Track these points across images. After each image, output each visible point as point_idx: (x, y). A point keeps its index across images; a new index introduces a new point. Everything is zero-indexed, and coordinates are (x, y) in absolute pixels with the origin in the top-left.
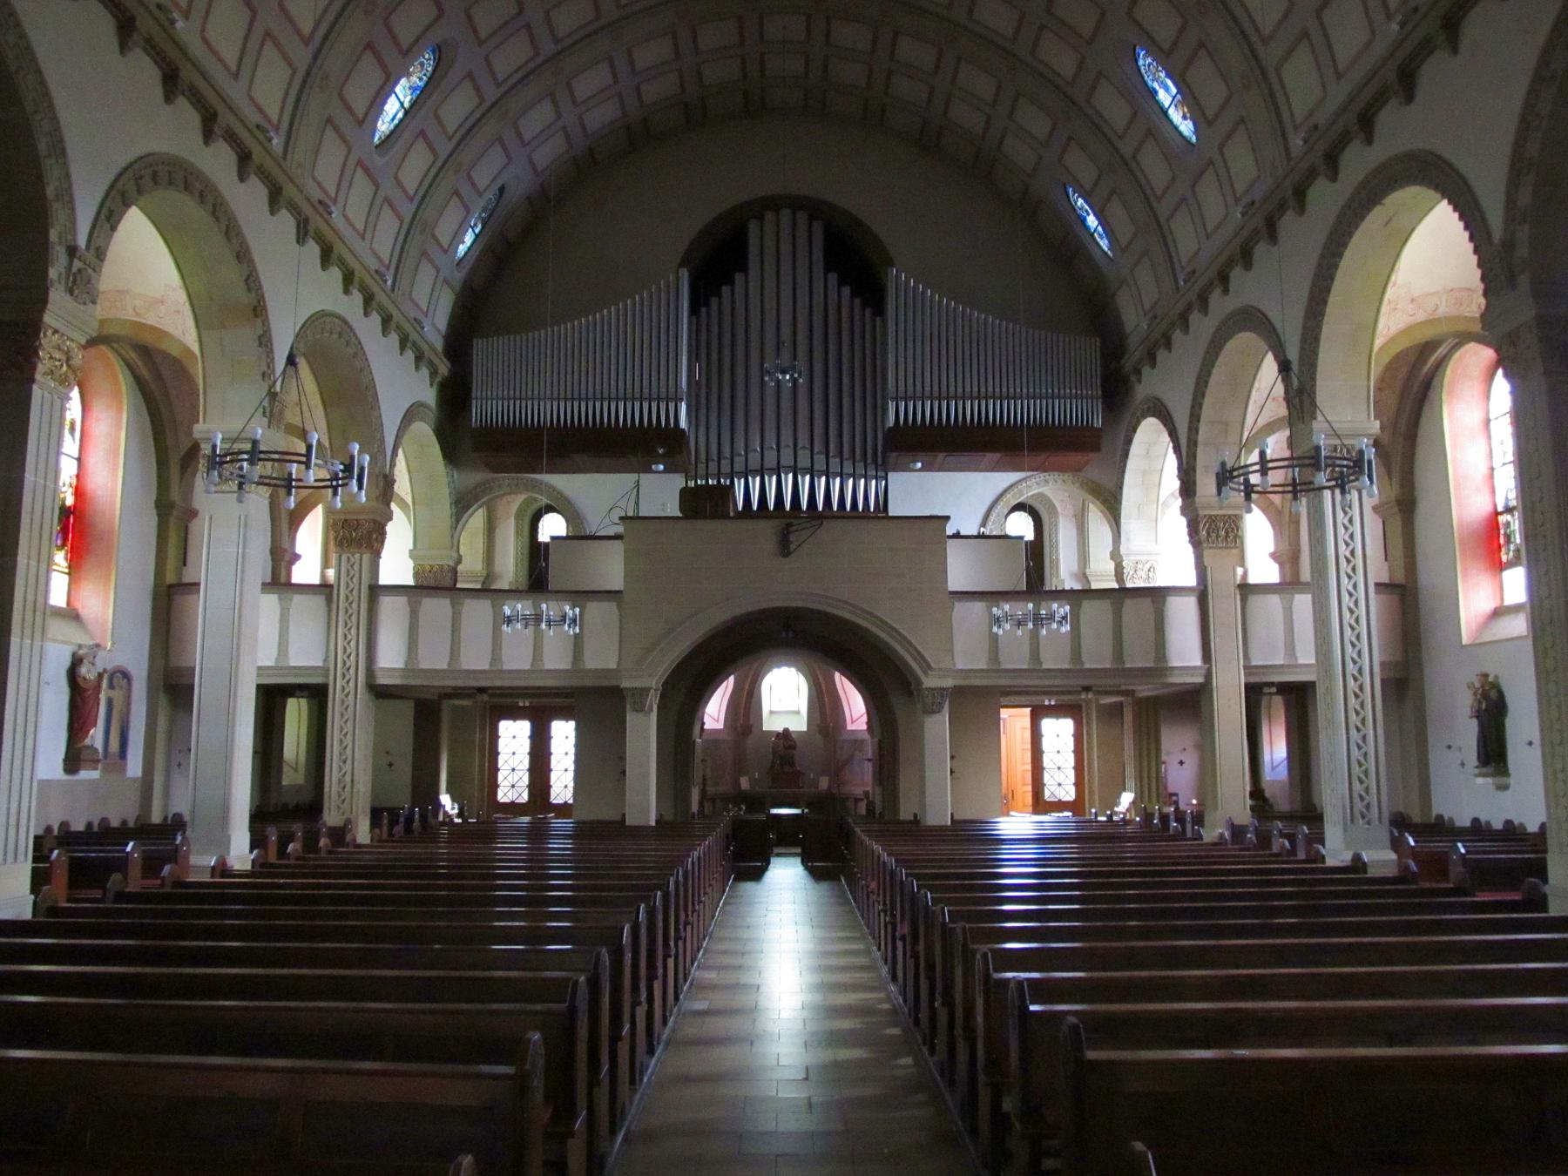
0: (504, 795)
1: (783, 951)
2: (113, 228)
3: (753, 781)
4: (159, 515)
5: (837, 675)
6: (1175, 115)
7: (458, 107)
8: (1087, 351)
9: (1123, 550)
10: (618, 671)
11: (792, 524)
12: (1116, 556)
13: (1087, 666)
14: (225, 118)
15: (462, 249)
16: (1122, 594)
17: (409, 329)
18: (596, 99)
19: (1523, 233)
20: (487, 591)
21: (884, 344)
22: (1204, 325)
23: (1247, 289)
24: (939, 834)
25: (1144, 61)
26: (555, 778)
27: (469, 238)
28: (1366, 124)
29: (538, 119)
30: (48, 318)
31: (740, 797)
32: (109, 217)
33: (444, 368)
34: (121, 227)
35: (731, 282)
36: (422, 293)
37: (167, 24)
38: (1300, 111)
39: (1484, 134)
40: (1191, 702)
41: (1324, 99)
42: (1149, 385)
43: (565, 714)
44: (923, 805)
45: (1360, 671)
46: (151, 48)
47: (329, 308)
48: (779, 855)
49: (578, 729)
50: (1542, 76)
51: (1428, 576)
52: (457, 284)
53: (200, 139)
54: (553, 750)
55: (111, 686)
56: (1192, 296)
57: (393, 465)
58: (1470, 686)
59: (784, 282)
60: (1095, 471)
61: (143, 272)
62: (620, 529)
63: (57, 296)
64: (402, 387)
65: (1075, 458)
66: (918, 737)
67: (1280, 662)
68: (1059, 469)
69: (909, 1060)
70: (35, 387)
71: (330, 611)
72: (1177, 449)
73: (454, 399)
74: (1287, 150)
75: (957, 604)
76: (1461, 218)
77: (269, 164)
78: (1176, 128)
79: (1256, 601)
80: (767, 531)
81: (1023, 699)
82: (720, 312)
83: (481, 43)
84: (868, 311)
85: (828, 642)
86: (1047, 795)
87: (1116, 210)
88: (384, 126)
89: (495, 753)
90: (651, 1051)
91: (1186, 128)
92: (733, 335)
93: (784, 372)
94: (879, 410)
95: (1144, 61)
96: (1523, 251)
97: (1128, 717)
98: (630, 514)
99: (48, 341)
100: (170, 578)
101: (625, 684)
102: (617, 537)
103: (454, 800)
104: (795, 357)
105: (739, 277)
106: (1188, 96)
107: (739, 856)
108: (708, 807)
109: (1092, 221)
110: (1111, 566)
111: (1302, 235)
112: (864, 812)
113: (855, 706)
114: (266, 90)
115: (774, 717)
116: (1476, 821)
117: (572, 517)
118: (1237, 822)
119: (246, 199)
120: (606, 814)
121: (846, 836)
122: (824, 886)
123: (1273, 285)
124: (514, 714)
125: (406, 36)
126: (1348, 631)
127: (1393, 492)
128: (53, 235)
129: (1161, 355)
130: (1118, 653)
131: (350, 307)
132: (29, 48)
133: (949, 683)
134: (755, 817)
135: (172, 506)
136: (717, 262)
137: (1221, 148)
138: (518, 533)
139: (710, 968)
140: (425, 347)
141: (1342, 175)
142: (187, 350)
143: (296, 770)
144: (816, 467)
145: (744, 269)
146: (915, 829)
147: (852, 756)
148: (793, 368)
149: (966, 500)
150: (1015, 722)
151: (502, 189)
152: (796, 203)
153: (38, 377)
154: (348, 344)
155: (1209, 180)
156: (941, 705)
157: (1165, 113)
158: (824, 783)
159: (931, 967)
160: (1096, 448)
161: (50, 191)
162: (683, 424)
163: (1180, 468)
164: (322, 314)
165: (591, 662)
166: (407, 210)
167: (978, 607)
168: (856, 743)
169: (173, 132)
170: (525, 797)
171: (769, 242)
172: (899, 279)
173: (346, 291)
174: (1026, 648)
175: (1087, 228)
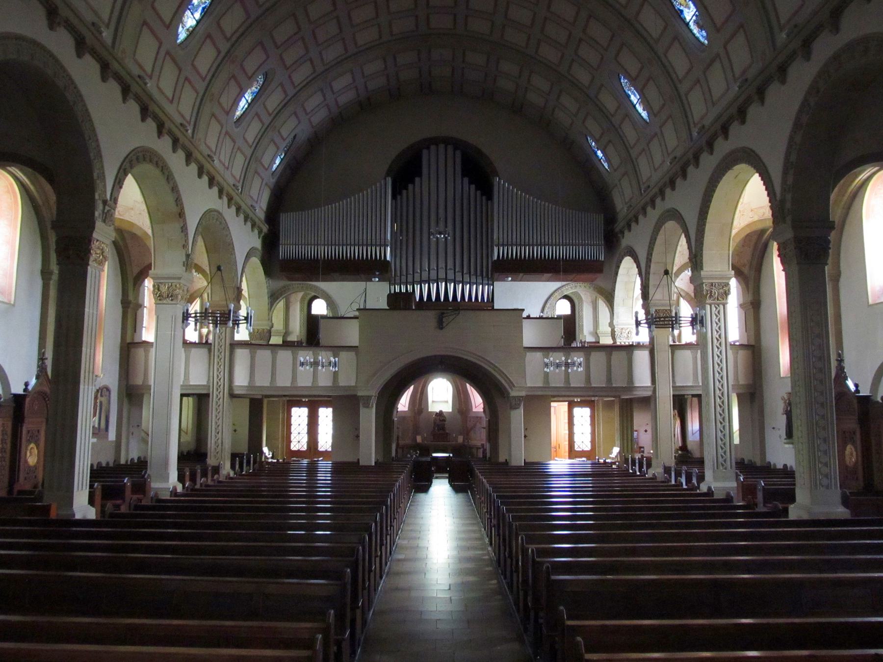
0: (294, 447)
1: (439, 530)
2: (121, 187)
3: (423, 439)
4: (123, 307)
5: (468, 385)
6: (640, 108)
7: (274, 101)
8: (598, 220)
9: (615, 322)
10: (355, 387)
11: (445, 310)
12: (611, 324)
13: (593, 385)
14: (168, 124)
15: (275, 166)
16: (614, 348)
17: (248, 211)
18: (344, 89)
19: (789, 197)
20: (287, 344)
21: (492, 216)
22: (653, 214)
23: (673, 200)
24: (518, 471)
25: (624, 81)
26: (294, 437)
27: (278, 162)
28: (725, 130)
29: (315, 101)
30: (95, 235)
31: (416, 446)
32: (119, 183)
33: (265, 228)
34: (124, 186)
35: (413, 183)
36: (254, 192)
37: (143, 86)
38: (697, 117)
39: (774, 144)
40: (648, 402)
41: (706, 114)
42: (627, 240)
43: (326, 404)
44: (510, 455)
45: (722, 394)
46: (138, 99)
47: (214, 207)
48: (437, 478)
49: (333, 412)
50: (797, 125)
51: (766, 341)
52: (272, 186)
53: (156, 135)
54: (320, 422)
55: (101, 396)
56: (648, 199)
57: (241, 281)
58: (783, 398)
59: (440, 180)
60: (601, 281)
61: (131, 202)
62: (357, 313)
63: (99, 224)
64: (245, 240)
65: (590, 276)
66: (508, 419)
67: (690, 384)
68: (583, 281)
69: (495, 582)
70: (89, 267)
71: (210, 357)
72: (640, 274)
73: (271, 242)
74: (691, 135)
75: (528, 354)
76: (764, 184)
77: (187, 143)
78: (640, 114)
79: (679, 354)
80: (431, 316)
81: (566, 399)
82: (407, 198)
83: (277, 47)
84: (484, 198)
85: (464, 371)
86: (577, 448)
87: (610, 149)
88: (238, 113)
89: (289, 425)
90: (381, 577)
91: (644, 114)
92: (414, 208)
93: (440, 234)
94: (490, 253)
95: (624, 81)
96: (788, 205)
97: (617, 408)
98: (362, 307)
99: (95, 245)
100: (129, 340)
101: (360, 394)
102: (355, 318)
103: (269, 450)
104: (446, 227)
105: (417, 179)
106: (644, 100)
107: (417, 479)
108: (400, 451)
109: (599, 153)
110: (610, 329)
111: (698, 176)
112: (481, 456)
113: (477, 401)
114: (184, 107)
115: (435, 404)
116: (785, 466)
117: (331, 304)
118: (667, 465)
119: (176, 161)
120: (350, 458)
121: (471, 472)
122: (460, 495)
123: (683, 198)
124: (299, 404)
125: (250, 69)
126: (717, 375)
127: (750, 298)
128: (97, 197)
129: (633, 225)
130: (609, 380)
131: (220, 205)
132: (87, 110)
133: (523, 394)
134: (424, 459)
135: (129, 303)
136: (405, 173)
137: (661, 127)
138: (301, 311)
139: (404, 539)
140: (257, 220)
141: (715, 153)
142: (147, 234)
143: (187, 433)
144: (457, 279)
145: (420, 175)
146: (505, 468)
147: (475, 426)
148: (444, 233)
149: (533, 299)
150: (559, 409)
151: (295, 137)
152: (447, 141)
153: (90, 263)
154: (221, 223)
155: (655, 142)
156: (519, 405)
157: (634, 106)
158: (460, 439)
159: (504, 540)
160: (600, 271)
161: (95, 175)
162: (388, 258)
163: (642, 285)
164: (209, 211)
165: (343, 382)
166: (248, 152)
167: (539, 355)
168: (478, 418)
169: (145, 135)
170: (305, 448)
171: (433, 160)
172: (499, 183)
173: (220, 197)
174: (563, 376)
175: (598, 157)
